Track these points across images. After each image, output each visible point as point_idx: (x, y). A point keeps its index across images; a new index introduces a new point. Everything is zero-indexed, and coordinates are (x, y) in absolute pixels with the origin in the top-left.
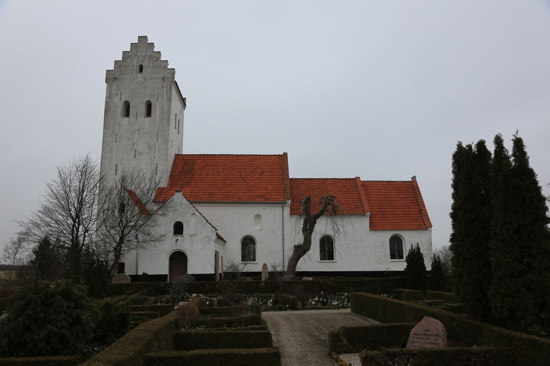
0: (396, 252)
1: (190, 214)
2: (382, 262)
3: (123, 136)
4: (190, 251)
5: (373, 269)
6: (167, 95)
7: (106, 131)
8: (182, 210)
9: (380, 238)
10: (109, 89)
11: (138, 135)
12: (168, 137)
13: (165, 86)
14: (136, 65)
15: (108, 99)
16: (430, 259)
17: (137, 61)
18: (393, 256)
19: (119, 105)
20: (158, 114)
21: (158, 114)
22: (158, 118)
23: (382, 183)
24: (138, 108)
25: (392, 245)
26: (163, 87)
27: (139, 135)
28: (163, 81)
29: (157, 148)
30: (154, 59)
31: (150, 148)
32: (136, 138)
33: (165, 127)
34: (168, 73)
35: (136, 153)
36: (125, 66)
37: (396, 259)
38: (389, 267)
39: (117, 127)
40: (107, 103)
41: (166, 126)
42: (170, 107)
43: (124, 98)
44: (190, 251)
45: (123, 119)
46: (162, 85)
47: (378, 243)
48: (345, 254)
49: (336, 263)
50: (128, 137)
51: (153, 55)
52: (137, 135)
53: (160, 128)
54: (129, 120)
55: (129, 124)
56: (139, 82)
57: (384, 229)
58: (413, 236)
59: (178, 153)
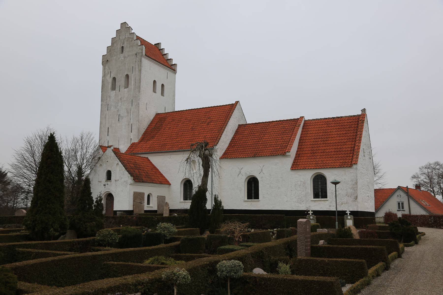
0: (320, 191)
1: (116, 164)
2: (303, 201)
3: (112, 105)
4: (115, 193)
5: (294, 208)
6: (139, 67)
7: (102, 103)
8: (111, 161)
9: (301, 177)
10: (104, 69)
11: (121, 103)
12: (139, 101)
13: (137, 61)
14: (119, 47)
15: (103, 78)
16: (354, 199)
17: (120, 44)
18: (316, 196)
19: (110, 82)
20: (133, 84)
21: (133, 84)
22: (133, 87)
23: (326, 120)
24: (121, 81)
25: (315, 184)
26: (136, 61)
27: (121, 103)
28: (136, 57)
29: (132, 112)
30: (130, 40)
31: (128, 112)
32: (120, 105)
33: (137, 94)
34: (139, 49)
35: (120, 117)
36: (113, 50)
37: (319, 198)
38: (309, 206)
39: (108, 99)
40: (103, 82)
41: (137, 93)
42: (140, 77)
43: (113, 76)
44: (115, 193)
45: (112, 92)
46: (135, 60)
47: (299, 183)
48: (267, 193)
49: (259, 202)
50: (115, 105)
51: (129, 37)
52: (120, 103)
53: (134, 96)
54: (115, 92)
55: (115, 95)
56: (121, 60)
57: (305, 169)
58: (336, 174)
59: (164, 112)
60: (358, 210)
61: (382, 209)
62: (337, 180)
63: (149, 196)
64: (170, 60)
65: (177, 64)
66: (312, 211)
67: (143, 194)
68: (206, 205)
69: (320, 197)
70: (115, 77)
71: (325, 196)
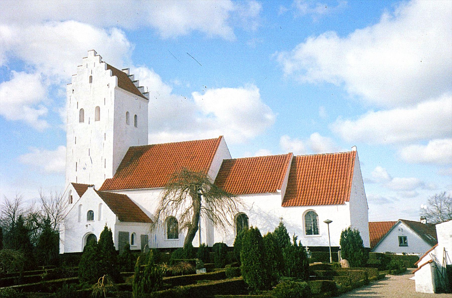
60: (148, 143)
61: (380, 245)
62: (329, 219)
63: (132, 235)
64: (141, 88)
65: (144, 87)
66: (308, 247)
67: (128, 233)
68: (362, 242)
69: (313, 233)
70: (82, 109)
71: (316, 232)
